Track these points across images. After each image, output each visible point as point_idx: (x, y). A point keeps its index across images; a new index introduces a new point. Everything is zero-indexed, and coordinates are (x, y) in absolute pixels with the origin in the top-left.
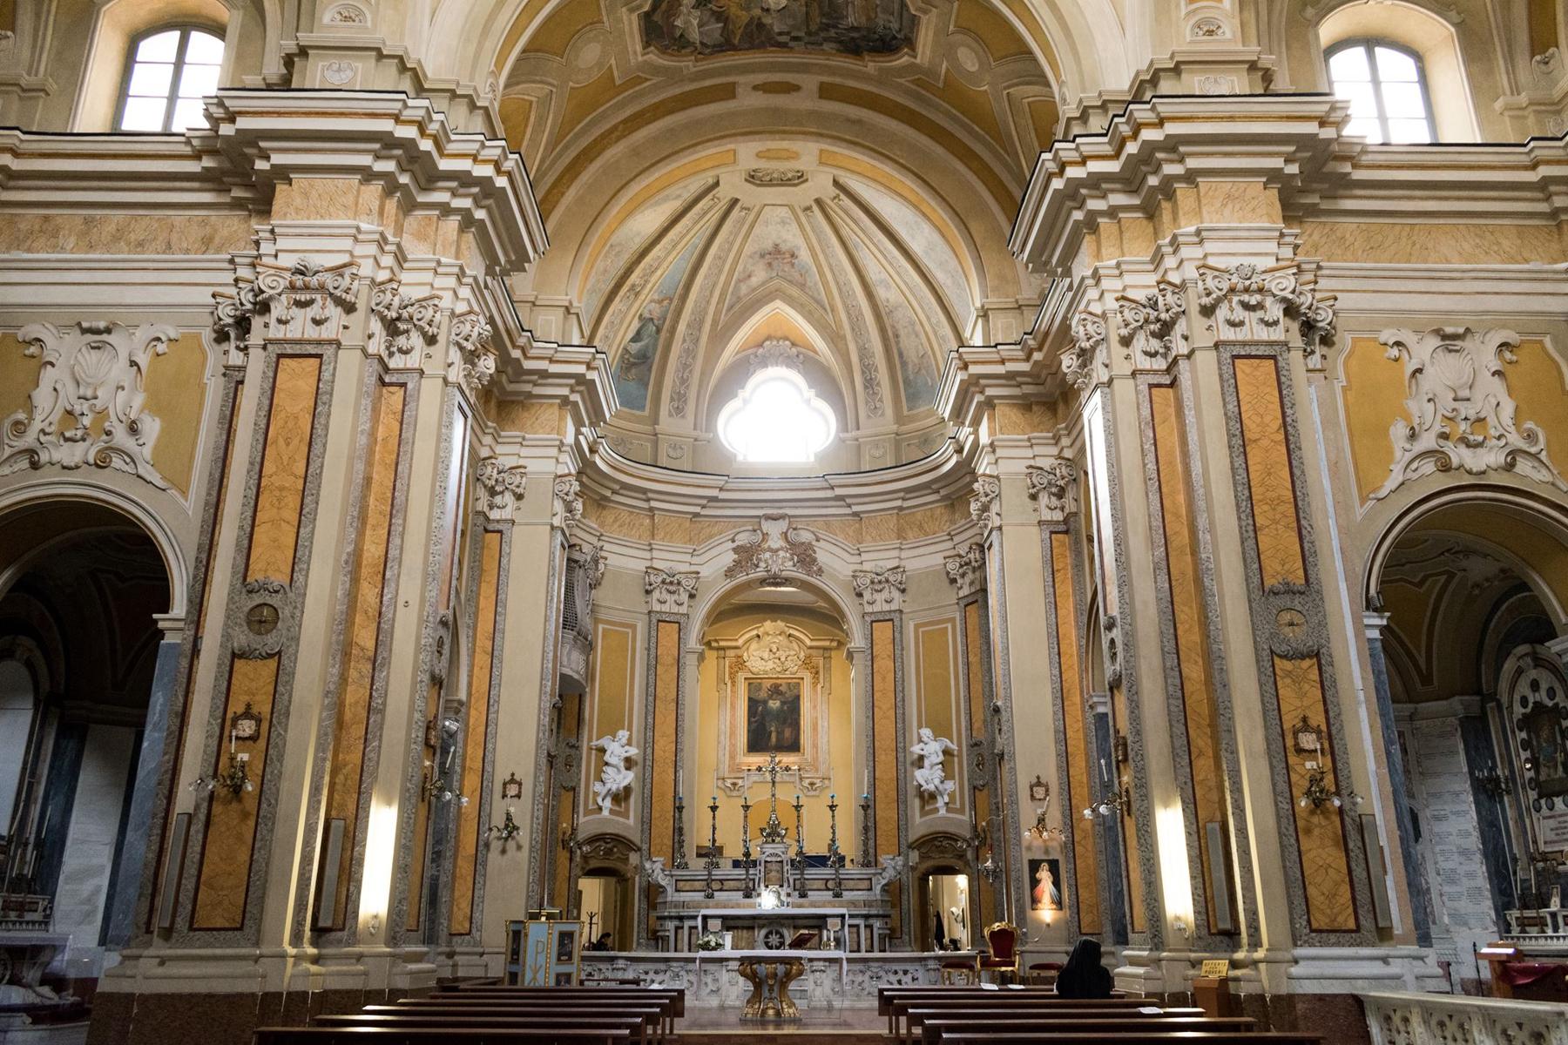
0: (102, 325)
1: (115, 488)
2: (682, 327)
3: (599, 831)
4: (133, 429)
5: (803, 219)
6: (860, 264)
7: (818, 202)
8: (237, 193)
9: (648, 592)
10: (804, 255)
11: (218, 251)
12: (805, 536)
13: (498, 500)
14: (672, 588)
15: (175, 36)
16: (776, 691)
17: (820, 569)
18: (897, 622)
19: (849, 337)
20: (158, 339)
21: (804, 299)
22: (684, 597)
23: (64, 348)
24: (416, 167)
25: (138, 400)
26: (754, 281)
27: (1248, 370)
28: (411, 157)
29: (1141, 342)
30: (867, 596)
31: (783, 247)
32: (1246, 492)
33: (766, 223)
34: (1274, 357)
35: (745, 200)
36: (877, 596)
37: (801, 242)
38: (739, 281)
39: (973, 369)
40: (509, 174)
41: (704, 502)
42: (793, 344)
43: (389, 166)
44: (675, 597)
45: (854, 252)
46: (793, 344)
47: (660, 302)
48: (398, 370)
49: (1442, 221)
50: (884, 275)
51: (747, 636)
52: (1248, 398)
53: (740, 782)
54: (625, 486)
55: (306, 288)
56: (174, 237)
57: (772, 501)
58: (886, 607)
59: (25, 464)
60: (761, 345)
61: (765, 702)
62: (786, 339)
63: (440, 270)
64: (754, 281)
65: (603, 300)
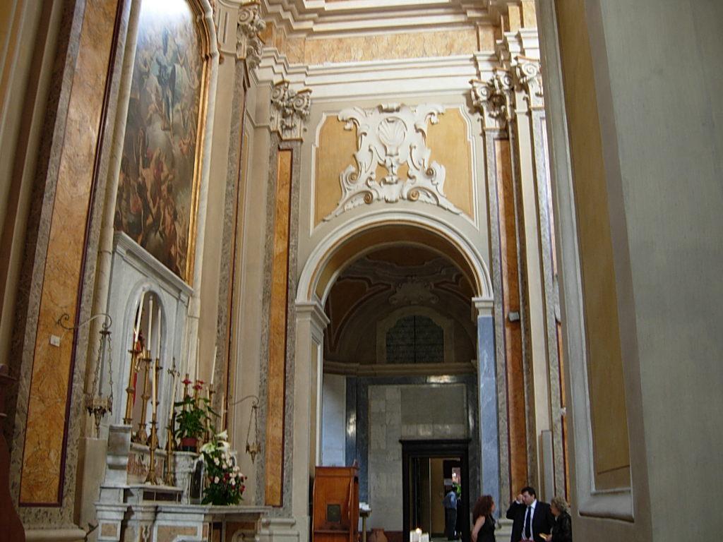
0: (395, 106)
1: (422, 214)
4: (430, 173)
8: (471, 14)
11: (458, 53)
15: (116, 254)
20: (432, 114)
23: (370, 123)
25: (427, 155)
49: (201, 152)
56: (427, 47)
59: (361, 201)
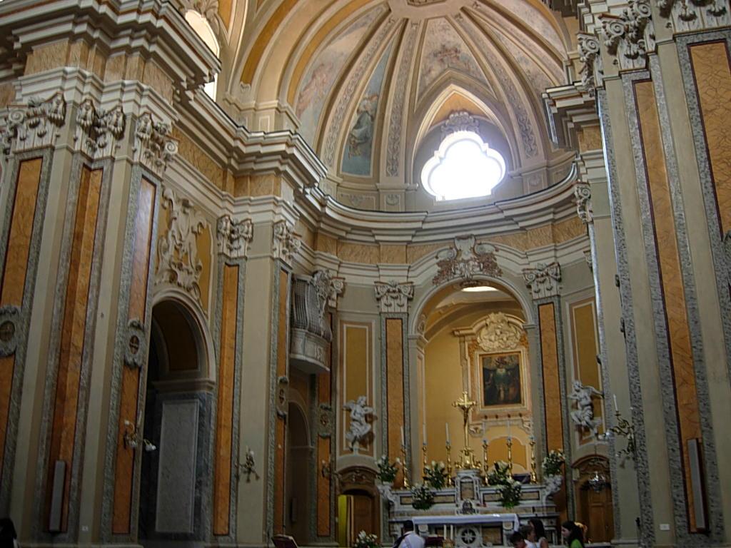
2: (388, 114)
3: (349, 465)
5: (457, 24)
6: (504, 49)
7: (463, 9)
9: (378, 300)
10: (464, 49)
12: (488, 249)
13: (236, 244)
14: (394, 295)
16: (502, 362)
17: (500, 271)
18: (556, 305)
19: (507, 102)
21: (471, 80)
22: (405, 301)
24: (102, 25)
26: (434, 74)
27: (702, 54)
28: (97, 21)
29: (623, 49)
30: (534, 287)
31: (449, 47)
32: (705, 155)
33: (433, 32)
34: (724, 40)
35: (412, 19)
36: (541, 286)
37: (460, 41)
38: (423, 75)
39: (559, 104)
40: (165, 17)
41: (413, 232)
42: (470, 114)
43: (83, 28)
44: (398, 301)
45: (498, 41)
46: (470, 114)
47: (370, 99)
48: (98, 160)
50: (522, 54)
51: (479, 326)
52: (704, 77)
53: (480, 427)
54: (354, 227)
55: (36, 115)
57: (470, 228)
58: (548, 294)
60: (447, 118)
61: (495, 371)
62: (464, 110)
63: (126, 89)
64: (434, 74)
65: (326, 106)
